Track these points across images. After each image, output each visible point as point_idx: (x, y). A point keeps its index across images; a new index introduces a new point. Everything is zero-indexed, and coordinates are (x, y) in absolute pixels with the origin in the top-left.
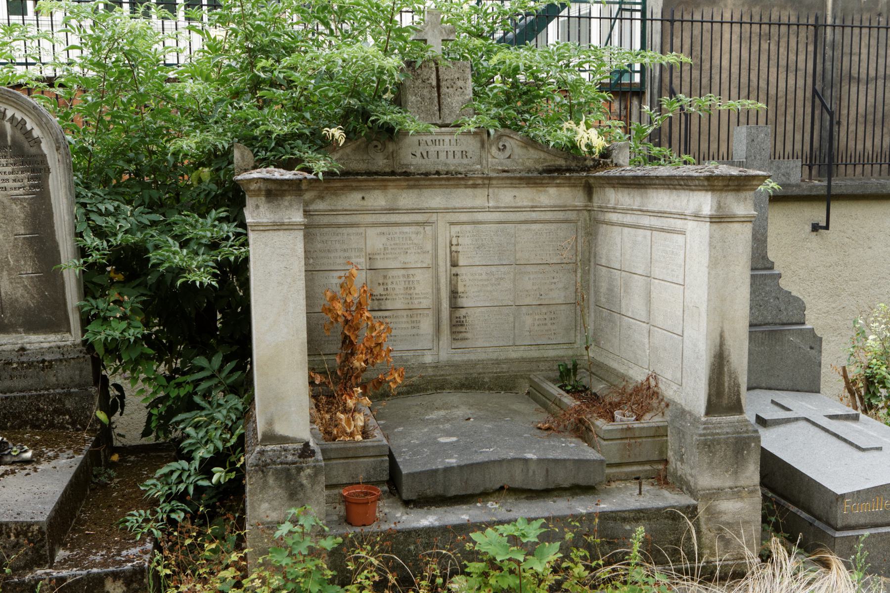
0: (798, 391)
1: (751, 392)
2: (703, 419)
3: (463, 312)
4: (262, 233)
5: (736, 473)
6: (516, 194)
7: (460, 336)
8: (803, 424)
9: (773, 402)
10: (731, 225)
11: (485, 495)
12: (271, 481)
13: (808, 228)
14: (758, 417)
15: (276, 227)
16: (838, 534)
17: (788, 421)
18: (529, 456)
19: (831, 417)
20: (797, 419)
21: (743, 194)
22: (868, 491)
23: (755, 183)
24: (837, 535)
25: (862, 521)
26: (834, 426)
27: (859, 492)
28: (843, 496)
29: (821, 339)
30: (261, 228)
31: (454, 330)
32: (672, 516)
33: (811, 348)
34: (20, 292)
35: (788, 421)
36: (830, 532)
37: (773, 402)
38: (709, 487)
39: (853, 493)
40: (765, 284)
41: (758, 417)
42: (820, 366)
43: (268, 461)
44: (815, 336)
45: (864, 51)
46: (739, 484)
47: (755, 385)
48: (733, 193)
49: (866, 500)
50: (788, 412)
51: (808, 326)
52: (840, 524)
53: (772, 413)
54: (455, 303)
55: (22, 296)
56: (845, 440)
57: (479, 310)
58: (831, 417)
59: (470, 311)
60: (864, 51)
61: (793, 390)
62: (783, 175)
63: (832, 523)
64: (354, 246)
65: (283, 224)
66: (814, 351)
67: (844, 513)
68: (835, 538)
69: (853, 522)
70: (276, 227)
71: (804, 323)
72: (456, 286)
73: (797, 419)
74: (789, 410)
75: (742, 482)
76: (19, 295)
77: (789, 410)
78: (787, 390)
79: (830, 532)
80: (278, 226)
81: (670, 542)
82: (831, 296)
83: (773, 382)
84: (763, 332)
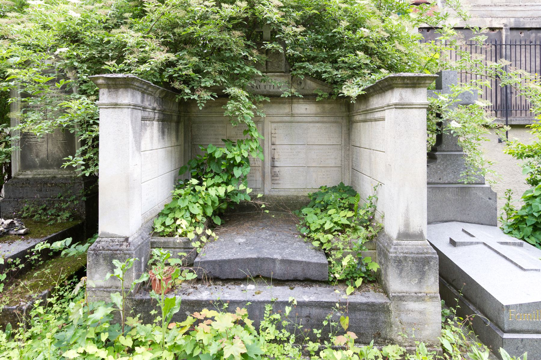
0: (482, 224)
1: (432, 226)
2: (395, 242)
3: (277, 169)
4: (106, 109)
5: (420, 282)
6: (308, 108)
7: (276, 182)
8: (482, 246)
9: (463, 230)
10: (410, 110)
11: (244, 280)
12: (101, 260)
13: (498, 141)
14: (451, 239)
15: (113, 106)
16: (506, 336)
17: (471, 243)
18: (275, 256)
19: (502, 243)
20: (478, 243)
21: (418, 90)
22: (529, 305)
23: (427, 82)
24: (504, 337)
25: (525, 327)
26: (503, 249)
27: (521, 305)
28: (508, 307)
29: (496, 194)
30: (105, 107)
31: (273, 178)
32: (372, 308)
33: (490, 199)
34: (56, 149)
35: (471, 243)
36: (499, 333)
37: (463, 230)
38: (400, 291)
39: (516, 305)
40: (458, 160)
41: (451, 239)
42: (496, 210)
43: (101, 248)
44: (492, 192)
45: (523, 59)
46: (422, 291)
47: (453, 219)
48: (411, 89)
49: (528, 312)
50: (472, 238)
51: (487, 185)
52: (506, 327)
53: (460, 237)
54: (274, 164)
55: (57, 152)
56: (511, 261)
57: (287, 168)
58: (502, 243)
59: (281, 169)
60: (523, 59)
61: (479, 224)
62: (467, 98)
63: (501, 326)
64: (221, 133)
65: (116, 104)
66: (491, 201)
67: (507, 320)
68: (503, 339)
69: (518, 328)
70: (113, 106)
71: (484, 184)
72: (274, 155)
73: (478, 243)
74: (473, 236)
75: (425, 290)
76: (55, 151)
77: (473, 236)
78: (475, 223)
79: (499, 333)
80: (115, 106)
81: (372, 327)
82: (511, 175)
83: (464, 218)
84: (457, 188)
